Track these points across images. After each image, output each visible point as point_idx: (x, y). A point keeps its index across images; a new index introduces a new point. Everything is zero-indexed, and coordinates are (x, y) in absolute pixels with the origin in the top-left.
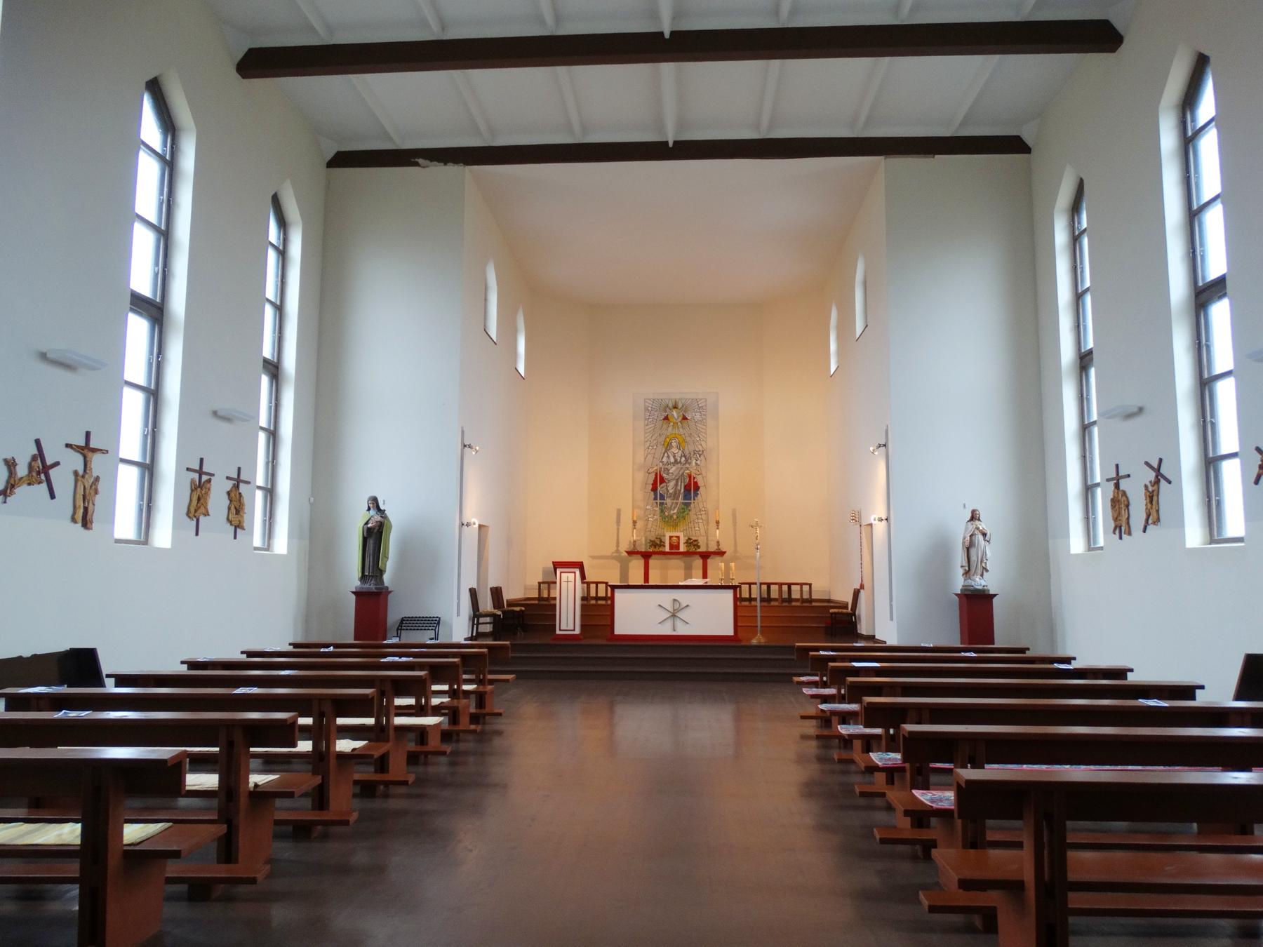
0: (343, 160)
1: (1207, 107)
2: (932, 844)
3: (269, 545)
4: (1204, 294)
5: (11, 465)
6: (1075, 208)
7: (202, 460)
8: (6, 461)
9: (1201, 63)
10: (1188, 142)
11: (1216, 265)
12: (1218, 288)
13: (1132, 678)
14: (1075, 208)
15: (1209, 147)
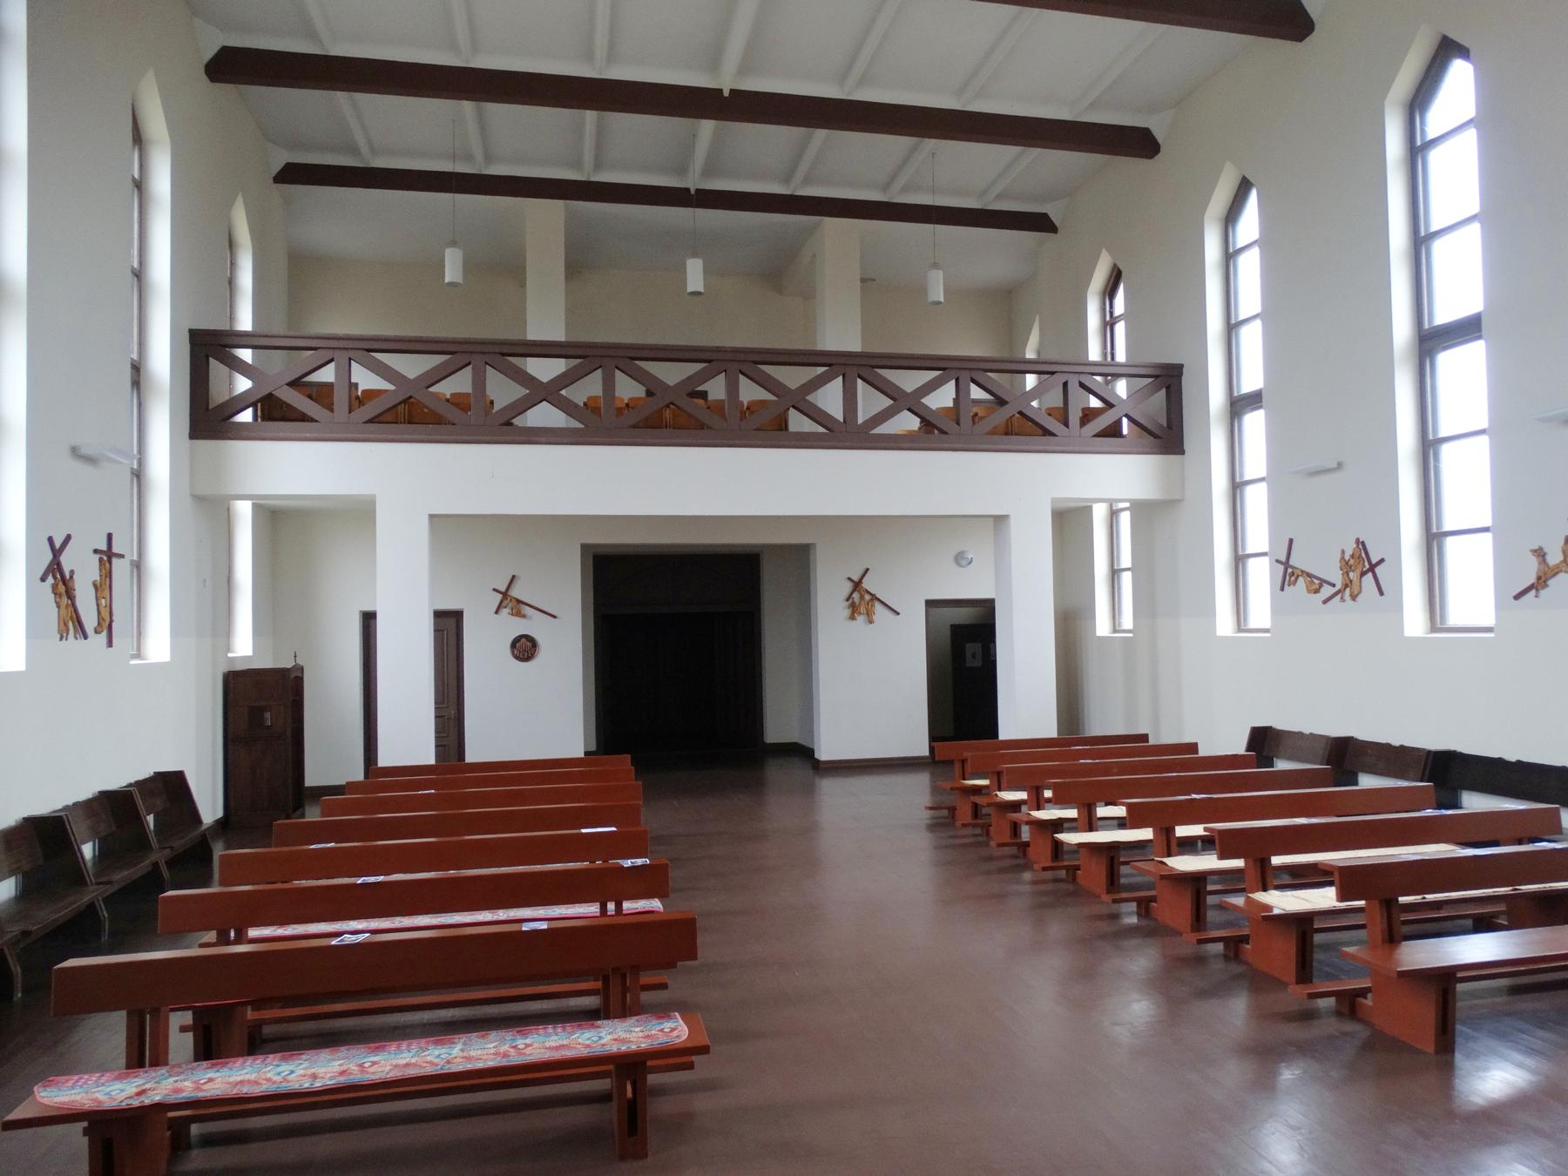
0: (293, 174)
1: (1249, 225)
2: (1077, 868)
3: (139, 649)
4: (1239, 405)
5: (1540, 553)
6: (1110, 292)
7: (110, 537)
8: (1534, 551)
9: (1244, 187)
10: (1229, 256)
11: (1252, 379)
12: (1254, 400)
13: (1203, 752)
14: (1110, 292)
15: (1249, 268)
